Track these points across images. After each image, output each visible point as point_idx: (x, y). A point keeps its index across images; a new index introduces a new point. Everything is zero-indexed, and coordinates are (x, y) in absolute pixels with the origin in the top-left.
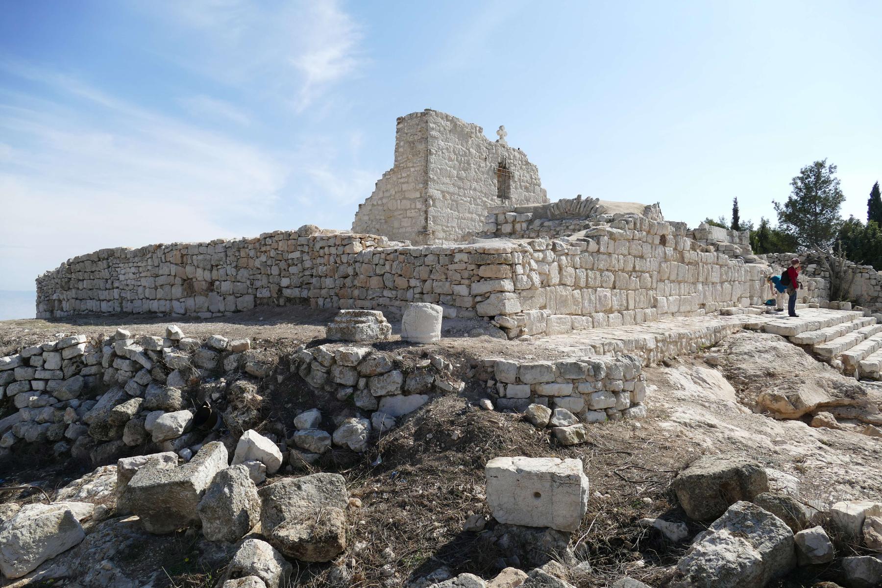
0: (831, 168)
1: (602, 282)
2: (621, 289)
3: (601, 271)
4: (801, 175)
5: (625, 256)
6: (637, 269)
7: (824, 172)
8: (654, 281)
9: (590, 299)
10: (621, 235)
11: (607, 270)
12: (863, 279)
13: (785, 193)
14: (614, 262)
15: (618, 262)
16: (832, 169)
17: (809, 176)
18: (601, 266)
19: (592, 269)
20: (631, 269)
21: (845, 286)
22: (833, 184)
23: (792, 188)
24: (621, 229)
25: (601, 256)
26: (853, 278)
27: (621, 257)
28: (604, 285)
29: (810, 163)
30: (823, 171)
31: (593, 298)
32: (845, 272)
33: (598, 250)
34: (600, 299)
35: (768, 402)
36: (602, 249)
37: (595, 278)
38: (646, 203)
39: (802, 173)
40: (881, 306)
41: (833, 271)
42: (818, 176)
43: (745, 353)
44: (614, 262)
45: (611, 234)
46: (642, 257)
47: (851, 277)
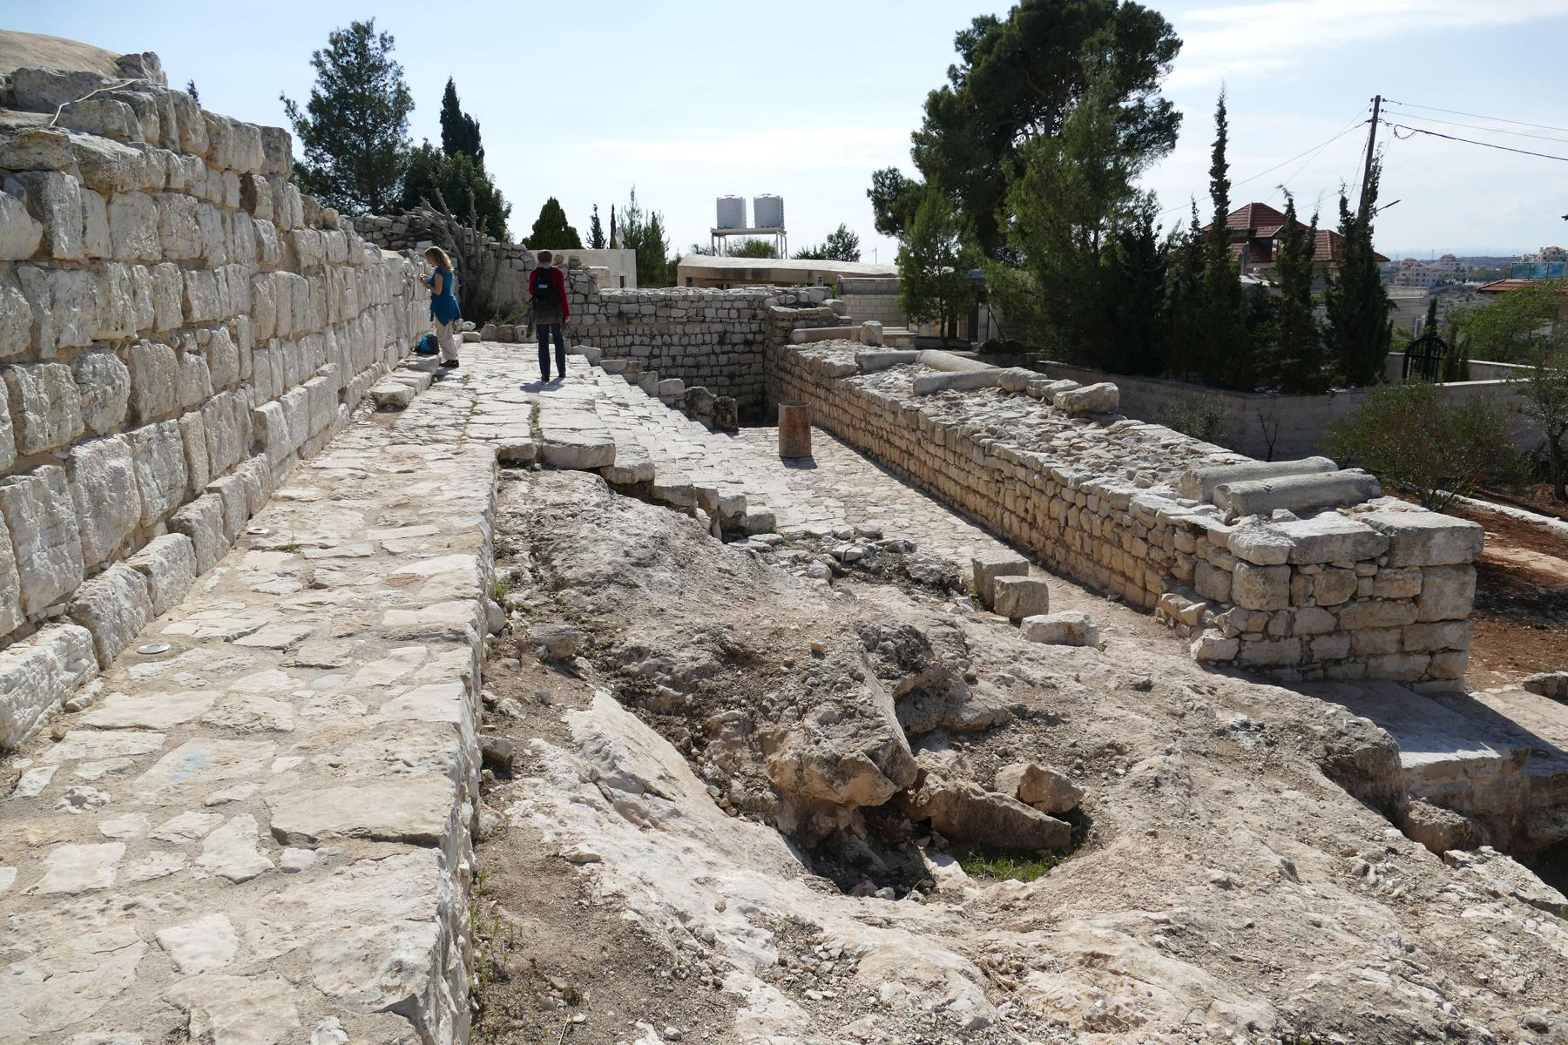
0: (383, 38)
1: (87, 412)
2: (159, 419)
3: (74, 356)
4: (331, 48)
5: (151, 265)
6: (197, 315)
7: (373, 44)
8: (246, 350)
9: (53, 524)
10: (134, 167)
11: (97, 345)
12: (514, 271)
13: (305, 85)
14: (121, 299)
15: (134, 296)
16: (387, 42)
17: (346, 53)
18: (73, 334)
19: (33, 357)
20: (178, 321)
21: (484, 286)
22: (391, 73)
23: (314, 73)
24: (118, 136)
25: (63, 277)
26: (497, 269)
27: (140, 271)
28: (98, 423)
29: (345, 26)
30: (370, 44)
31: (64, 510)
32: (484, 255)
33: (45, 249)
34: (97, 501)
35: (817, 786)
36: (64, 245)
37: (57, 401)
38: (123, 51)
39: (334, 42)
40: (1567, 505)
41: (462, 253)
42: (362, 51)
43: (610, 580)
44: (121, 299)
45: (89, 164)
46: (201, 264)
47: (492, 266)
